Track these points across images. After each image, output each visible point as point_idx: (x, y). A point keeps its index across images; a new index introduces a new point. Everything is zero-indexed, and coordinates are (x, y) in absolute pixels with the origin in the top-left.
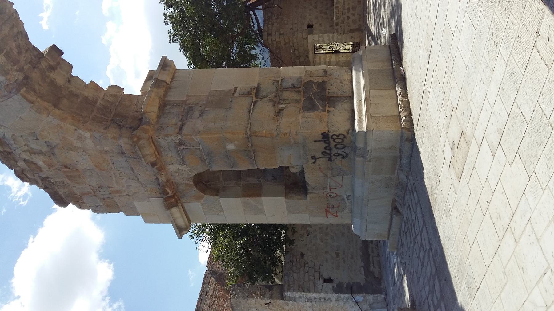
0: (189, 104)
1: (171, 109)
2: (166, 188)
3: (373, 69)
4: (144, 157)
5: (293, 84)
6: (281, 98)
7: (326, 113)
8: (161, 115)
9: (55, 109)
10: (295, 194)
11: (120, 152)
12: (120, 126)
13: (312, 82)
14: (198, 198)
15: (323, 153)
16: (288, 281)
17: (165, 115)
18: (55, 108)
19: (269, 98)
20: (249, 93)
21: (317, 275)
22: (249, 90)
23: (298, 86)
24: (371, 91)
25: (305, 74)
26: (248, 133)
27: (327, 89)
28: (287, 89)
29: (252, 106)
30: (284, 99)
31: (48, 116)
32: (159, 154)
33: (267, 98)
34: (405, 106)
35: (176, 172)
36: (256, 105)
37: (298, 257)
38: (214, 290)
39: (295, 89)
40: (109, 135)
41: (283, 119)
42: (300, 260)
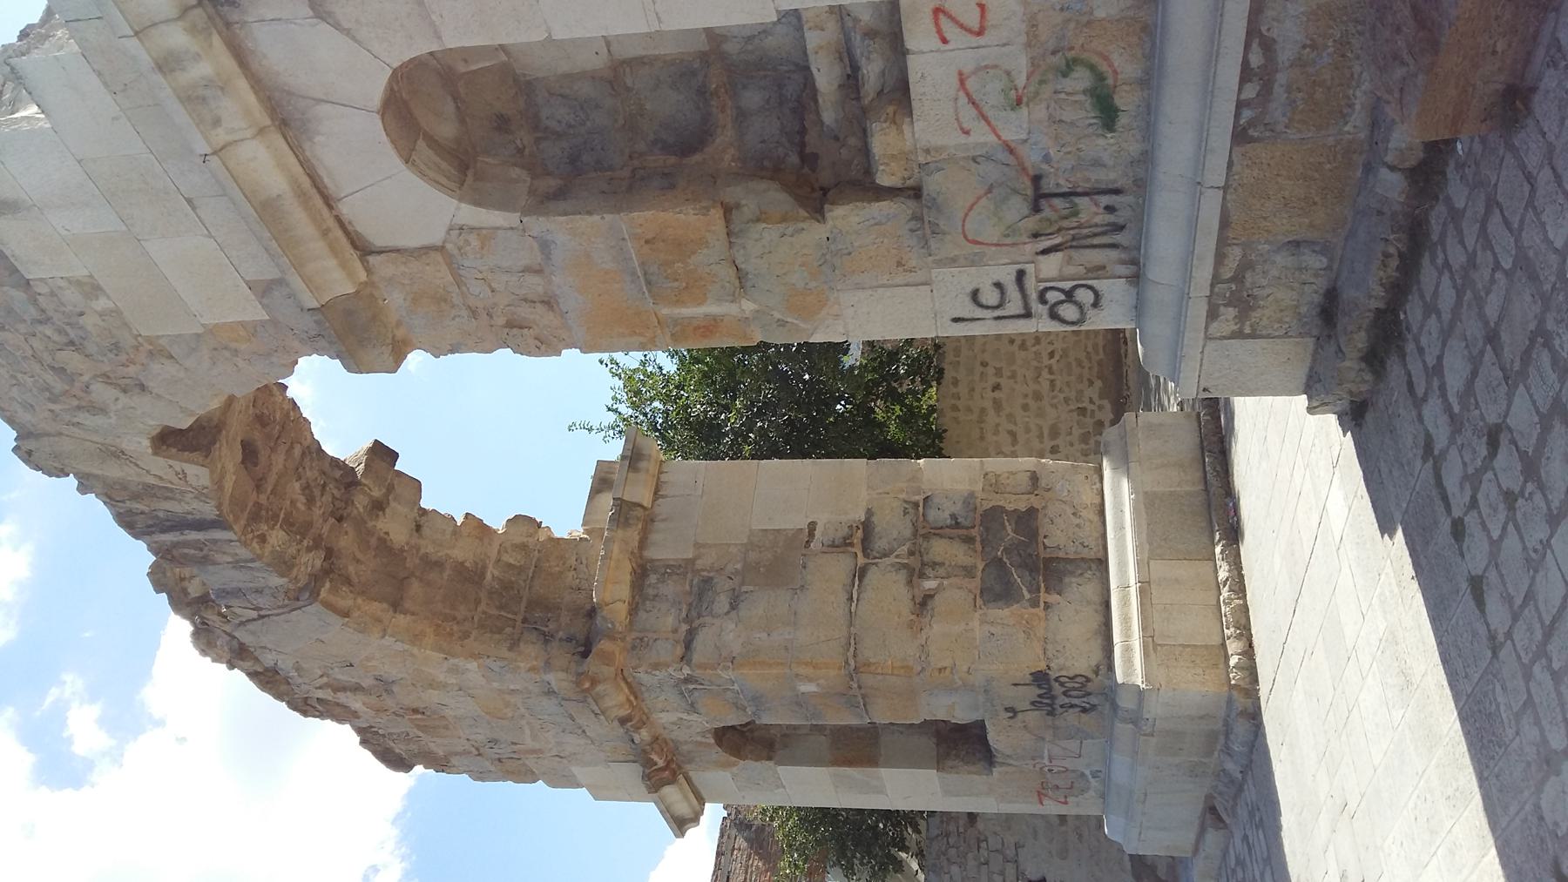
2: (652, 757)
4: (603, 713)
5: (953, 516)
7: (1040, 611)
9: (397, 615)
10: (963, 760)
11: (546, 690)
12: (544, 634)
14: (725, 766)
17: (648, 602)
18: (395, 612)
19: (897, 557)
20: (846, 542)
23: (967, 523)
24: (1152, 562)
25: (984, 485)
27: (1042, 532)
29: (857, 583)
31: (383, 637)
32: (636, 698)
33: (892, 559)
36: (866, 581)
38: (746, 873)
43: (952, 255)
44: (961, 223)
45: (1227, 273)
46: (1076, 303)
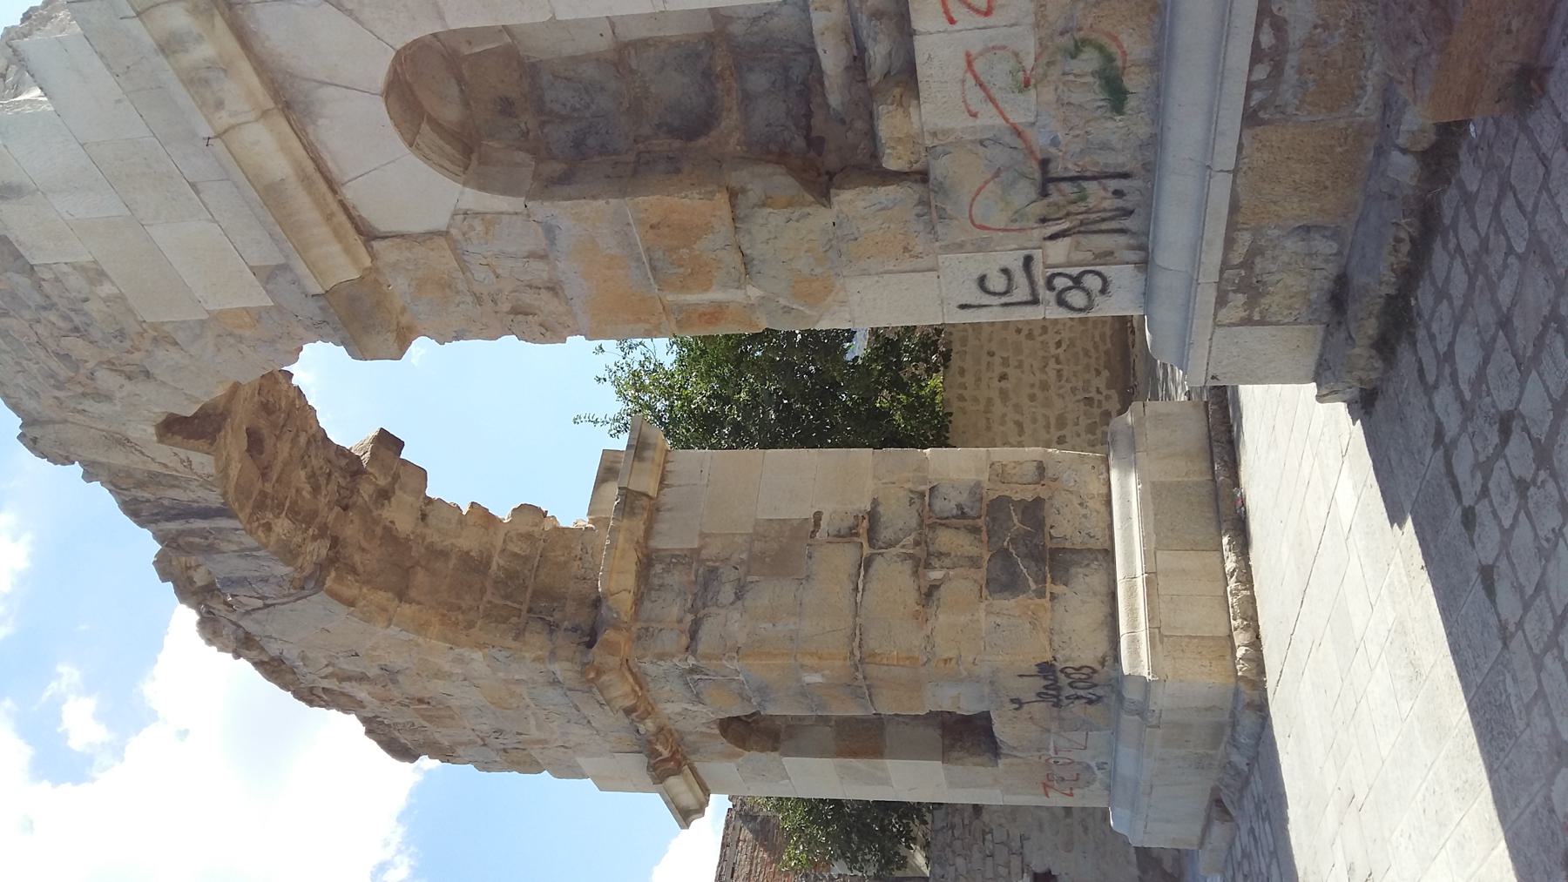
0: (708, 560)
1: (665, 575)
2: (657, 747)
3: (1162, 479)
5: (959, 507)
6: (931, 549)
7: (1046, 602)
8: (643, 593)
10: (968, 751)
12: (549, 624)
13: (1008, 499)
14: (730, 756)
15: (1039, 694)
16: (943, 877)
19: (903, 547)
20: (852, 532)
21: (1016, 862)
22: (850, 521)
23: (972, 513)
26: (855, 656)
28: (943, 522)
29: (862, 573)
30: (941, 554)
31: (388, 626)
32: (641, 688)
33: (897, 550)
34: (1245, 613)
35: (680, 714)
36: (872, 571)
37: (966, 815)
38: (752, 864)
39: (966, 522)
40: (527, 655)
41: (941, 617)
42: (971, 823)
43: (958, 240)
44: (967, 209)
45: (1236, 258)
46: (1083, 289)
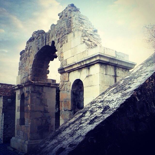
5: (48, 122)
